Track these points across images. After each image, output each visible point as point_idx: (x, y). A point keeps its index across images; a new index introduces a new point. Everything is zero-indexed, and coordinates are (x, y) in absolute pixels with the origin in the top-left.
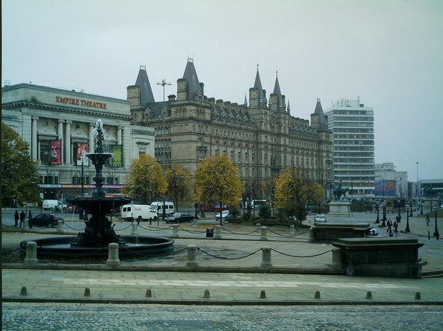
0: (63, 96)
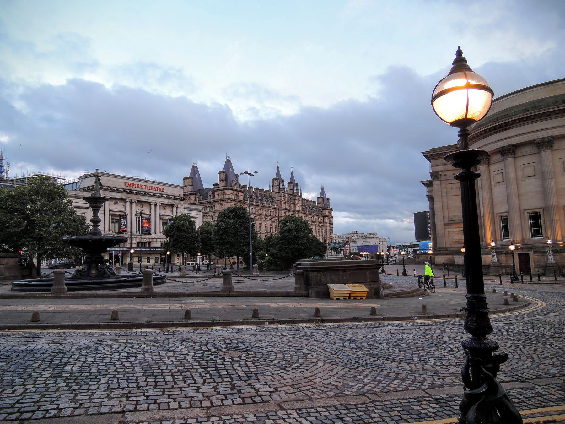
0: (130, 182)
